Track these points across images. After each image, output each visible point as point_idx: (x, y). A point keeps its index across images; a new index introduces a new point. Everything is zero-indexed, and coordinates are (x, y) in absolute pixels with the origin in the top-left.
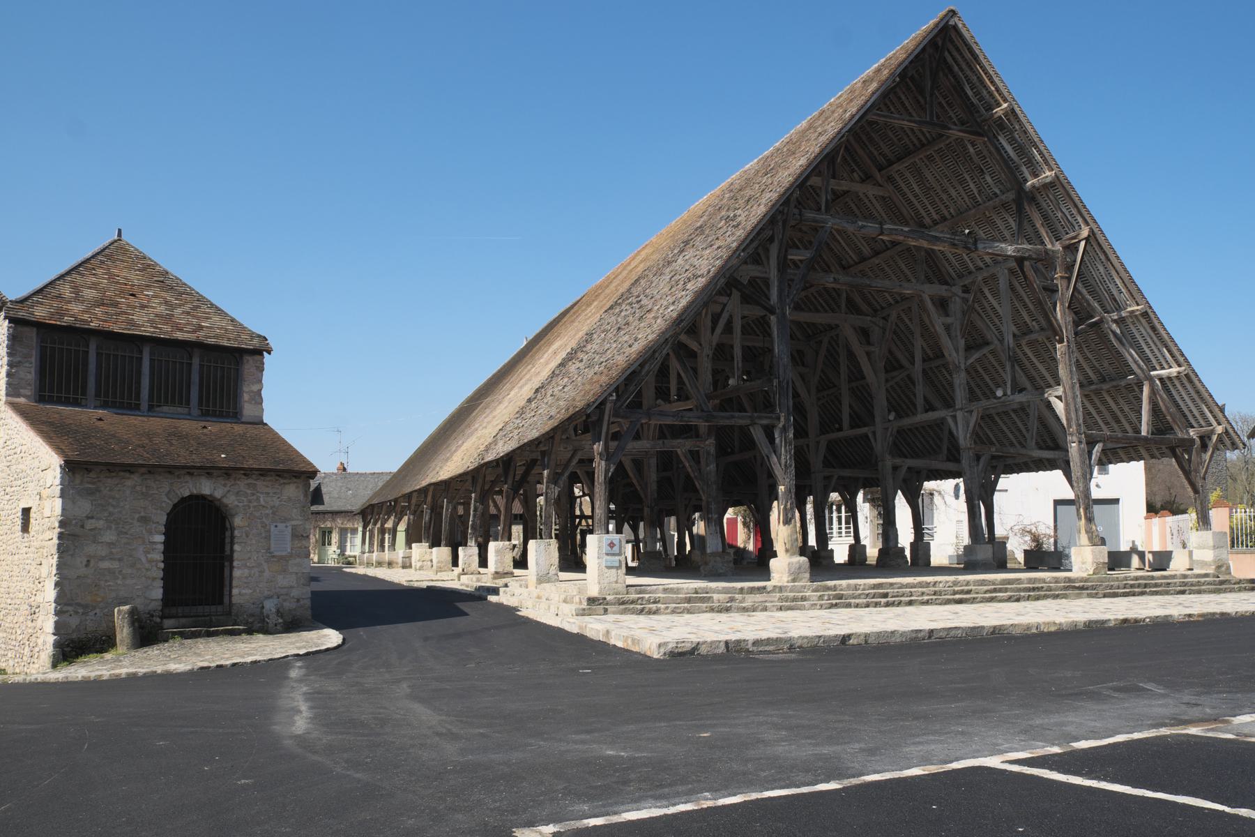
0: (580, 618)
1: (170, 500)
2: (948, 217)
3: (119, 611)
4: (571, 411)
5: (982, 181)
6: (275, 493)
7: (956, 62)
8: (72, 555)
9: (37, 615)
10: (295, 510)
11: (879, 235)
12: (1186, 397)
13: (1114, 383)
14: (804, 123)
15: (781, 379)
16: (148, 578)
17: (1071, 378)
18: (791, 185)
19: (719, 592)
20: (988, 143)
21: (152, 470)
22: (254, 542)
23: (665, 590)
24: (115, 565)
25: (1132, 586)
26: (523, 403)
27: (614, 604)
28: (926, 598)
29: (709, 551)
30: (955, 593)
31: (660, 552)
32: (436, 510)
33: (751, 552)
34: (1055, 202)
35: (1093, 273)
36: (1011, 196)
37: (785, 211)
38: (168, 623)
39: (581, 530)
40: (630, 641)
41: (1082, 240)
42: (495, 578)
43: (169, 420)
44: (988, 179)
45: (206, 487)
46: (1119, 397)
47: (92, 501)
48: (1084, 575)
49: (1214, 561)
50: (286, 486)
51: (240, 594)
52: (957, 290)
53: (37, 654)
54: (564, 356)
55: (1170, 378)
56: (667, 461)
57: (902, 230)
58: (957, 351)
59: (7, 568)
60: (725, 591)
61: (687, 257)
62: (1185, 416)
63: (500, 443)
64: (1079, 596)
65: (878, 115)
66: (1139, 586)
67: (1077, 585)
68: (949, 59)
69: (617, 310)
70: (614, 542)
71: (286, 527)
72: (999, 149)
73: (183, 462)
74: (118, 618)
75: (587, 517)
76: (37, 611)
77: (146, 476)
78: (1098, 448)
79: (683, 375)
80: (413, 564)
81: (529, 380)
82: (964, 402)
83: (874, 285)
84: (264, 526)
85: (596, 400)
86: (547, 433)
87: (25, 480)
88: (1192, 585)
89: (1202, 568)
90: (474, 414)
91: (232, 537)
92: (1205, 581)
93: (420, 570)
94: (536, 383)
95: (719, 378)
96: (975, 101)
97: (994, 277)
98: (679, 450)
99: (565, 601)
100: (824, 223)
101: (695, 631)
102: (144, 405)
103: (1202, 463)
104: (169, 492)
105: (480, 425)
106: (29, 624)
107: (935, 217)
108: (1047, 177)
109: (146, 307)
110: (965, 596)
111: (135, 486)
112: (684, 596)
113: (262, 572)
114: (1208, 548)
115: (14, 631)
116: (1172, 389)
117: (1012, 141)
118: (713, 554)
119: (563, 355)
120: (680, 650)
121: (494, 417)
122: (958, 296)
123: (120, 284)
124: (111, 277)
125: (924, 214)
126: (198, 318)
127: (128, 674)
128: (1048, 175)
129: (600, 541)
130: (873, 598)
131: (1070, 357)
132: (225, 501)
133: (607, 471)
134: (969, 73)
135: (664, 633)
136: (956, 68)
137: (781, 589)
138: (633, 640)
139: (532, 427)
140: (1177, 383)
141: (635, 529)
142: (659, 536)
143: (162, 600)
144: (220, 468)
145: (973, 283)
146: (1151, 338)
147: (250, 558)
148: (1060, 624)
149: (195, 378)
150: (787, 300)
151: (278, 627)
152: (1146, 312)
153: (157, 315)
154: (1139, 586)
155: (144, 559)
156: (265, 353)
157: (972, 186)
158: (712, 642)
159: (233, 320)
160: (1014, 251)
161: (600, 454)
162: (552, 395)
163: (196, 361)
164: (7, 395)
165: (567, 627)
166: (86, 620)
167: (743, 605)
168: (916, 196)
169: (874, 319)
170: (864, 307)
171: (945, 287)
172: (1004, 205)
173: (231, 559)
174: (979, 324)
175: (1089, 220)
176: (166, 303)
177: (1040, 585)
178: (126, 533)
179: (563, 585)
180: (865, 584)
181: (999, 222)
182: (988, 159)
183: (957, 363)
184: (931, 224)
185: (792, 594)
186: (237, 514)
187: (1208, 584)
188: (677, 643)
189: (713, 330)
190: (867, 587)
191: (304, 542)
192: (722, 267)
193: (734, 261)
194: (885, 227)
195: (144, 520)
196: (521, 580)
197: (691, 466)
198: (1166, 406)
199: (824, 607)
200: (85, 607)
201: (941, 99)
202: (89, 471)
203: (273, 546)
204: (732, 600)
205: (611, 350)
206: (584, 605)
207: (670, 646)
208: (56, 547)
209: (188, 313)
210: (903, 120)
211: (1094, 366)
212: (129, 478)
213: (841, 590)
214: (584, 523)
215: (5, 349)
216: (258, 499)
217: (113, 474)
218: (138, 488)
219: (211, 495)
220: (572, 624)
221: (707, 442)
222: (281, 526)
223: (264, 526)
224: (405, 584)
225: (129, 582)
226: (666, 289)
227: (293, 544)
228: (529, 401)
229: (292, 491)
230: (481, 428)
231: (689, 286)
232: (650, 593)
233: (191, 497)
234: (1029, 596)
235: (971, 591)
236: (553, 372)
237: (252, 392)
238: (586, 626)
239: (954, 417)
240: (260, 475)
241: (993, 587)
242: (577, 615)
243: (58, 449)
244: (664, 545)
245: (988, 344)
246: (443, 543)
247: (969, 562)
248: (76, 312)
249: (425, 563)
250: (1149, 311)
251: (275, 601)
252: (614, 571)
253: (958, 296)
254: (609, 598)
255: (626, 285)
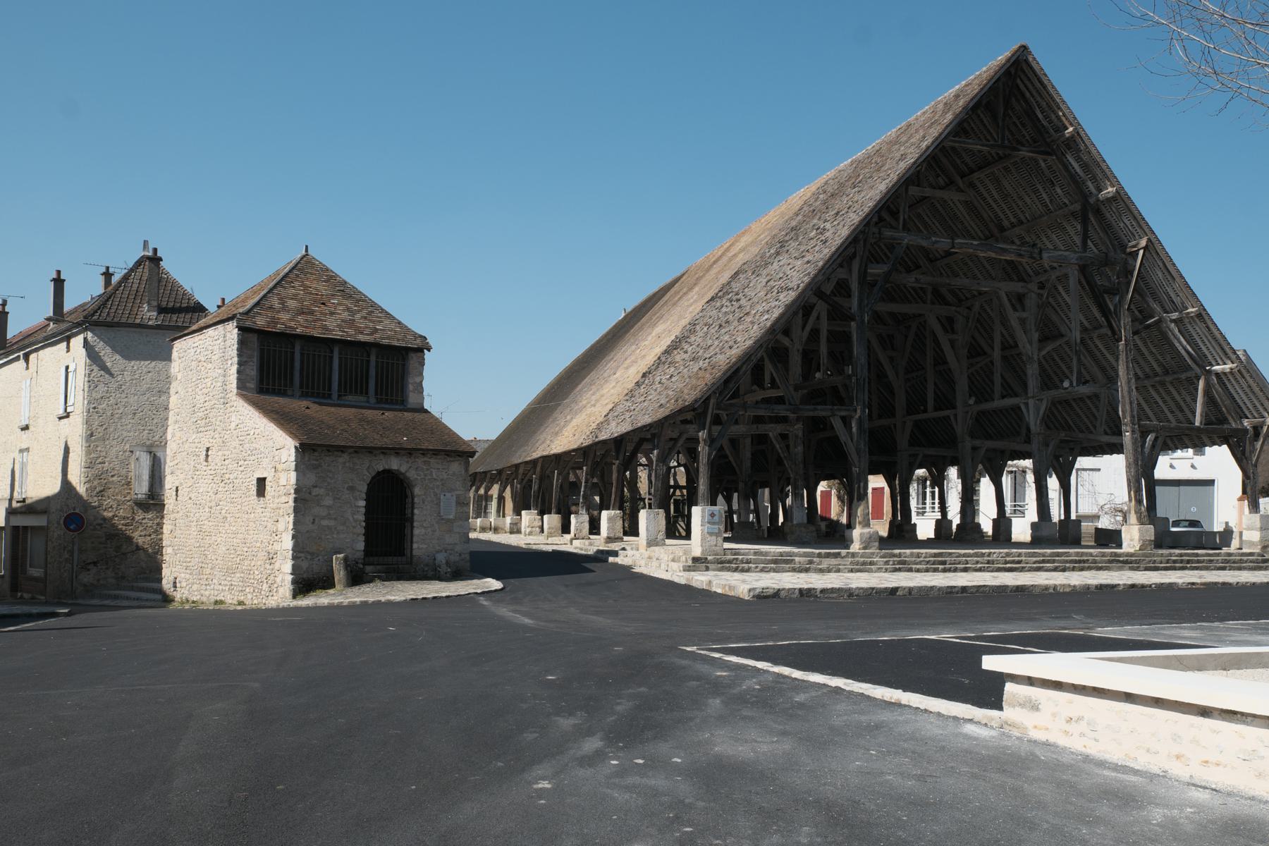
0: (687, 573)
1: (370, 474)
2: (1025, 221)
3: (337, 558)
4: (680, 404)
5: (1053, 192)
6: (443, 469)
7: (1028, 89)
8: (303, 515)
9: (275, 560)
10: (458, 483)
11: (951, 248)
12: (1240, 391)
13: (1175, 376)
14: (893, 132)
15: (859, 377)
16: (354, 534)
17: (1128, 374)
18: (871, 211)
19: (801, 556)
20: (1056, 161)
21: (357, 450)
22: (428, 507)
23: (755, 554)
24: (332, 523)
25: (1175, 562)
26: (631, 385)
27: (714, 563)
28: (979, 566)
29: (795, 522)
30: (1006, 562)
31: (752, 522)
32: (545, 479)
33: (844, 525)
34: (1117, 214)
35: (1153, 277)
36: (1077, 207)
37: (866, 231)
38: (369, 569)
39: (674, 500)
40: (727, 588)
41: (1141, 249)
42: (607, 542)
43: (353, 410)
44: (1059, 191)
45: (395, 464)
46: (1182, 388)
47: (316, 473)
48: (1132, 550)
49: (1261, 541)
50: (452, 463)
51: (418, 548)
52: (1033, 286)
53: (275, 589)
54: (669, 343)
55: (1225, 374)
56: (761, 439)
57: (972, 244)
58: (1031, 343)
59: (243, 524)
60: (805, 555)
61: (781, 263)
62: (1240, 407)
63: (613, 424)
64: (1120, 569)
65: (955, 142)
66: (1182, 561)
67: (1121, 559)
68: (1022, 86)
69: (718, 304)
70: (715, 513)
71: (452, 496)
72: (1066, 167)
73: (379, 444)
74: (336, 564)
75: (681, 488)
76: (275, 556)
77: (353, 455)
78: (1150, 438)
79: (775, 375)
80: (523, 530)
81: (635, 362)
82: (1036, 390)
83: (953, 284)
84: (436, 495)
85: (702, 396)
86: (660, 420)
87: (259, 456)
88: (1234, 562)
89: (1249, 548)
90: (578, 389)
91: (413, 503)
92: (1248, 559)
93: (529, 535)
94: (643, 366)
95: (807, 375)
96: (1045, 123)
97: (1066, 276)
98: (771, 434)
99: (673, 560)
100: (900, 240)
101: (777, 582)
102: (335, 396)
103: (1254, 449)
104: (368, 467)
105: (588, 403)
106: (268, 566)
107: (1013, 220)
108: (1109, 192)
109: (334, 313)
110: (1014, 566)
111: (345, 463)
112: (771, 558)
113: (434, 531)
114: (1256, 530)
115: (252, 572)
116: (1227, 383)
117: (1078, 159)
118: (799, 525)
119: (666, 342)
120: (765, 594)
121: (602, 396)
122: (1033, 292)
123: (313, 294)
124: (306, 288)
125: (1002, 216)
126: (373, 322)
127: (361, 602)
128: (1110, 190)
129: (703, 511)
130: (933, 564)
131: (1127, 354)
132: (408, 474)
133: (709, 455)
134: (1039, 99)
135: (753, 583)
136: (1028, 95)
137: (853, 555)
138: (730, 587)
139: (643, 412)
140: (1231, 378)
141: (728, 500)
142: (752, 507)
143: (364, 551)
144: (406, 449)
145: (1048, 280)
146: (1206, 337)
147: (425, 520)
148: (1074, 586)
149: (373, 372)
150: (866, 309)
151: (448, 575)
152: (1200, 314)
153: (343, 321)
154: (1182, 561)
155: (351, 519)
156: (425, 350)
157: (1044, 196)
158: (789, 589)
159: (399, 323)
160: (1077, 259)
161: (705, 440)
162: (660, 383)
163: (373, 358)
164: (238, 388)
165: (676, 580)
166: (313, 564)
167: (820, 567)
168: (995, 201)
169: (958, 309)
170: (949, 298)
171: (1021, 284)
172: (1073, 214)
173: (411, 521)
174: (1054, 318)
175: (1147, 231)
176: (348, 309)
177: (1086, 558)
178: (339, 499)
179: (670, 548)
180: (926, 553)
181: (1069, 228)
182: (1058, 173)
183: (1030, 355)
184: (1009, 226)
185: (862, 559)
186: (416, 485)
187: (1251, 562)
188: (763, 589)
189: (803, 328)
190: (928, 556)
191: (465, 508)
192: (809, 284)
193: (820, 278)
194: (956, 241)
195: (352, 489)
196: (631, 544)
197: (781, 448)
198: (1221, 399)
199: (889, 570)
200: (312, 554)
201: (1015, 119)
202: (314, 450)
203: (442, 511)
204: (811, 562)
205: (714, 347)
206: (690, 563)
207: (758, 591)
208: (292, 508)
209: (365, 318)
210: (977, 145)
211: (1158, 360)
212: (340, 457)
213: (905, 557)
214: (678, 492)
215: (236, 352)
216: (431, 474)
217: (330, 453)
218: (347, 464)
219: (398, 470)
220: (680, 577)
221: (795, 427)
222: (448, 495)
223: (436, 495)
224: (524, 546)
225: (342, 536)
226: (763, 293)
227: (457, 510)
228: (638, 384)
229: (456, 467)
230: (589, 405)
231: (782, 296)
232: (743, 555)
233: (385, 471)
234: (1074, 567)
235: (1022, 561)
236: (659, 358)
237: (416, 383)
238: (692, 578)
239: (1026, 404)
240: (434, 454)
241: (1042, 558)
242: (684, 571)
243: (292, 434)
244: (758, 517)
245: (1062, 336)
246: (553, 511)
247: (1040, 537)
248: (286, 321)
249: (534, 529)
250: (1203, 313)
251: (445, 555)
252: (714, 538)
253: (1033, 292)
254: (709, 558)
255: (725, 277)
